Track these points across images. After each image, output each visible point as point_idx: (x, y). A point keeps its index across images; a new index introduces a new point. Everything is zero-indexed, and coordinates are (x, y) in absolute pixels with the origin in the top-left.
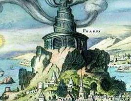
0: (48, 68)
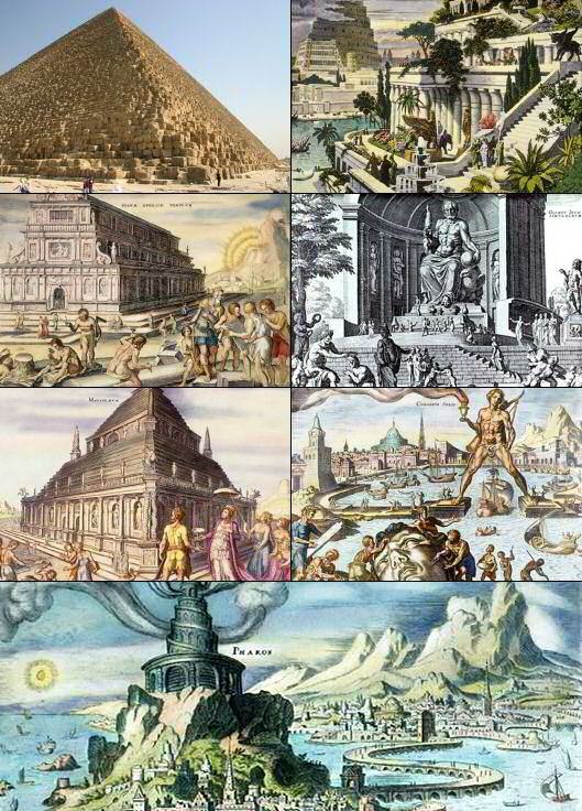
0: (153, 735)
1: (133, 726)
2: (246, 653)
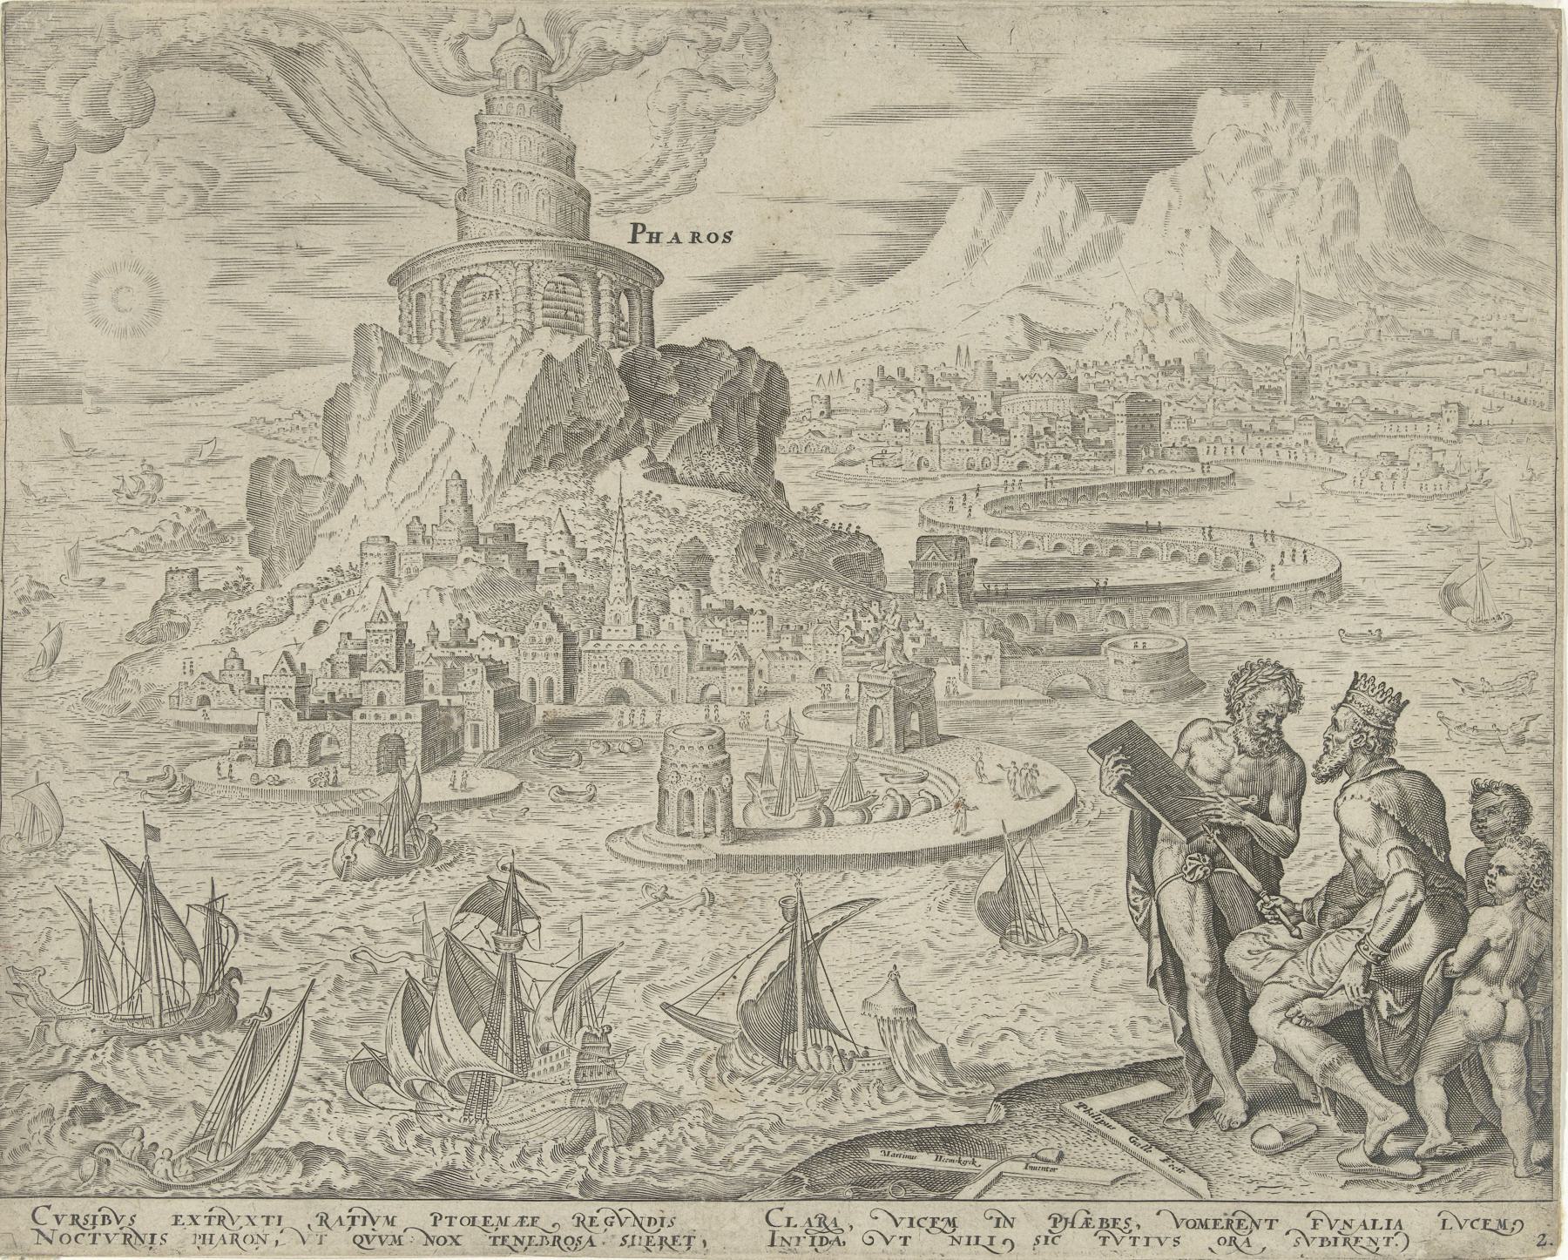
0: (419, 459)
1: (367, 433)
2: (664, 239)
